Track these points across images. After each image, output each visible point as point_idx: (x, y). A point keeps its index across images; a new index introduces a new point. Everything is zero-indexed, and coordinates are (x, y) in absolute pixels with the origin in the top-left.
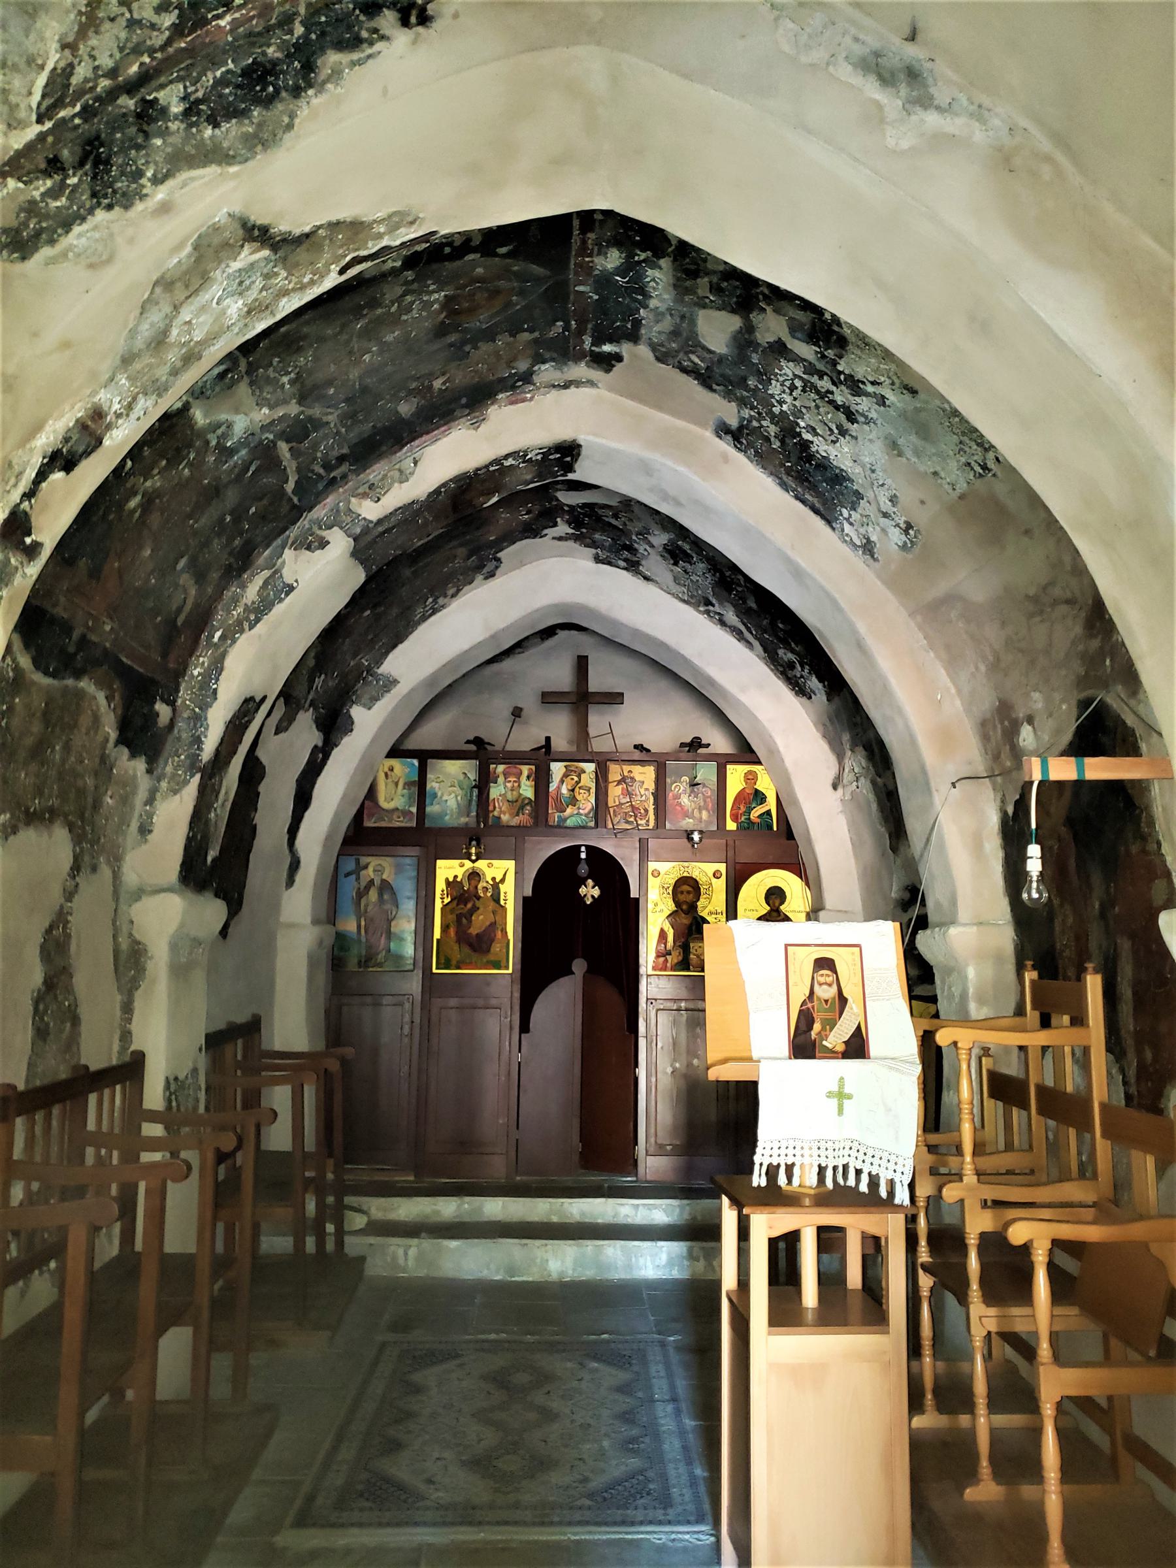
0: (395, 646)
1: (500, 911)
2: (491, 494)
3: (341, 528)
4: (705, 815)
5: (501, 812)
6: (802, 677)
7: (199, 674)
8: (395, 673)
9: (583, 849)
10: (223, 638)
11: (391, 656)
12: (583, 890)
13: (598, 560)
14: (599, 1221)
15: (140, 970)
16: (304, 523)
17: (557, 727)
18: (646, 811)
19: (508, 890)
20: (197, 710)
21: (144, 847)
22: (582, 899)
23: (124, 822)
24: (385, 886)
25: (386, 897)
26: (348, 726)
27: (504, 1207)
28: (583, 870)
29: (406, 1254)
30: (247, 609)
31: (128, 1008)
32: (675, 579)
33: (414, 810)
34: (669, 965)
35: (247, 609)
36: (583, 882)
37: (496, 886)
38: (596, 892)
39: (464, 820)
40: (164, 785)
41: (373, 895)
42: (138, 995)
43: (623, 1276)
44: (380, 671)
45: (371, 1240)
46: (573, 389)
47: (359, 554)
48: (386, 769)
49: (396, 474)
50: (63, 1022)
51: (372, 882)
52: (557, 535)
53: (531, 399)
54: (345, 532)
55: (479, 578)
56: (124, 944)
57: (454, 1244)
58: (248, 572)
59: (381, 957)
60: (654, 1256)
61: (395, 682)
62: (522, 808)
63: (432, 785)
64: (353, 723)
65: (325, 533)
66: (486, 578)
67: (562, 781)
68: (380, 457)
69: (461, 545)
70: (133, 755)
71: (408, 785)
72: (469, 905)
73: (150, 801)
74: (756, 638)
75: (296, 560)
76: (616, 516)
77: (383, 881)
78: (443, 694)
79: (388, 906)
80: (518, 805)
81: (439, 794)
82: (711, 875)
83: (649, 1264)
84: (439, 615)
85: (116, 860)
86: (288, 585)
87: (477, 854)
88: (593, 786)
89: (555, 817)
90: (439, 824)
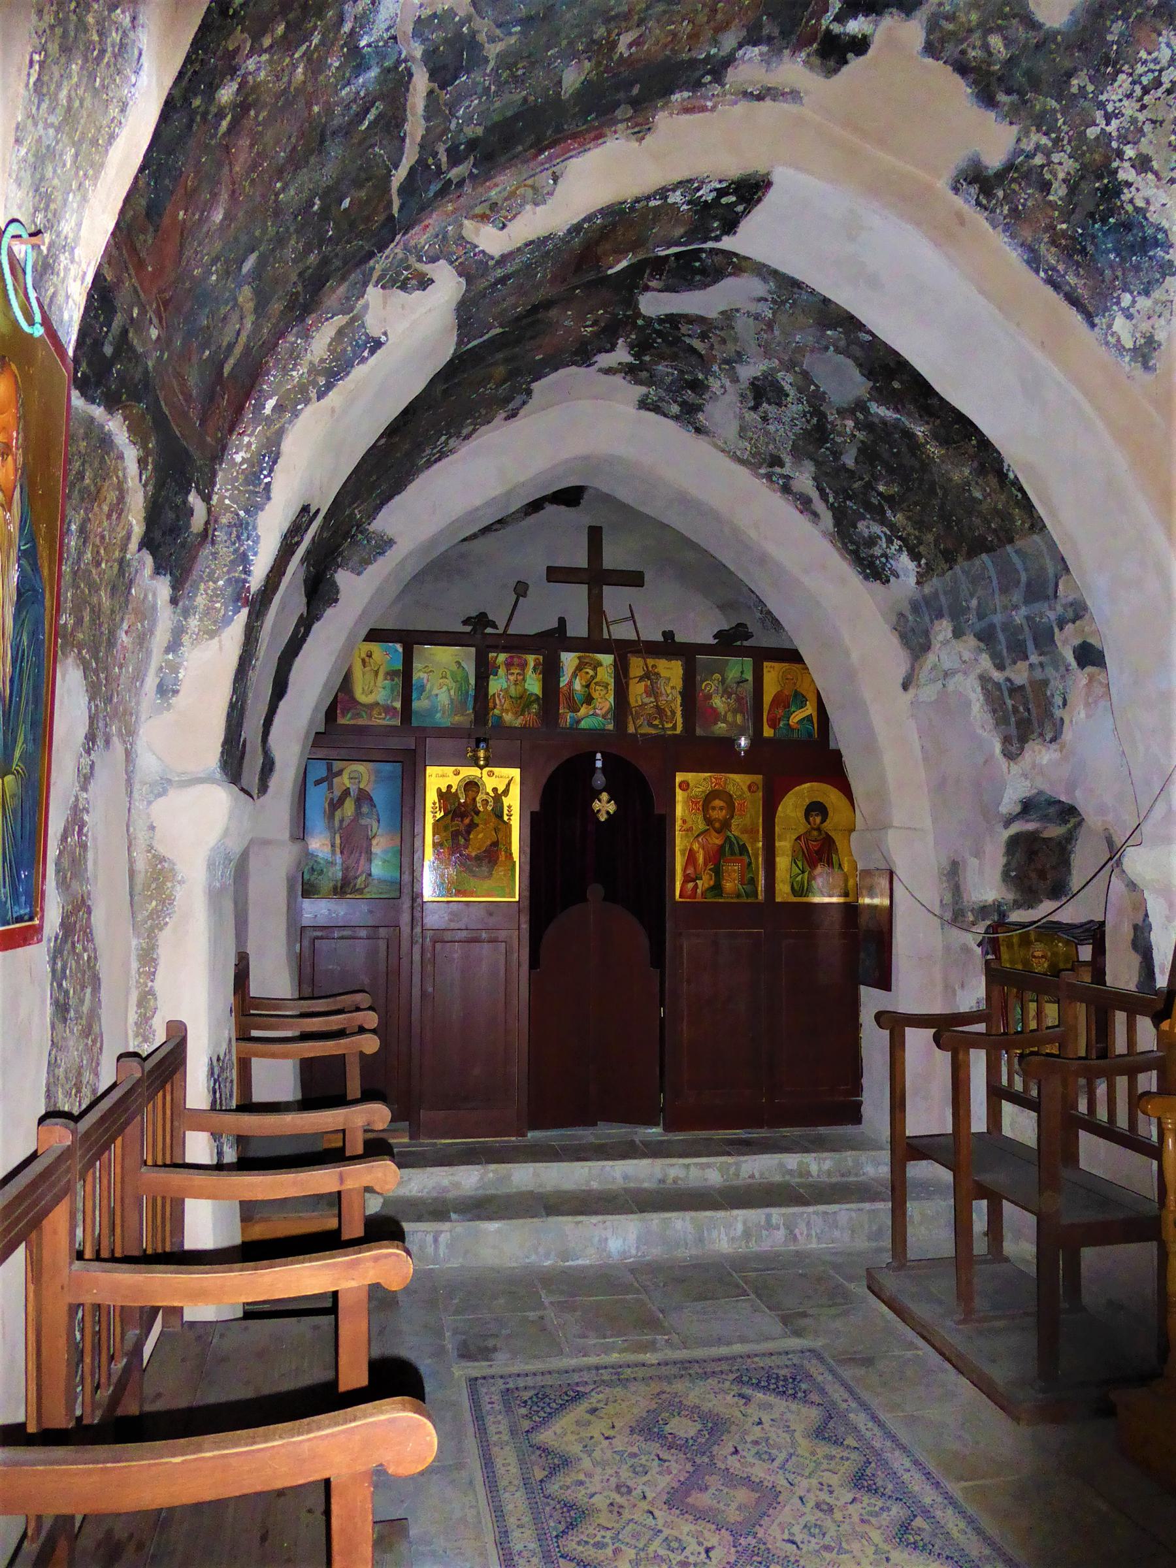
0: (390, 498)
2: (620, 253)
3: (451, 263)
4: (739, 718)
5: (502, 710)
6: (885, 555)
7: (244, 460)
8: (390, 532)
9: (599, 756)
10: (279, 408)
11: (384, 510)
13: (644, 404)
15: (166, 901)
16: (395, 250)
17: (570, 606)
18: (673, 713)
19: (513, 801)
20: (242, 513)
21: (167, 716)
22: (595, 814)
23: (139, 676)
25: (365, 809)
26: (332, 597)
27: (536, 1174)
28: (599, 780)
29: (436, 1240)
30: (313, 370)
31: (148, 958)
32: (743, 429)
33: (398, 705)
34: (699, 891)
36: (596, 795)
37: (498, 797)
38: (612, 807)
39: (457, 718)
40: (193, 623)
41: (349, 807)
42: (165, 938)
46: (768, 103)
47: (466, 314)
48: (363, 655)
49: (530, 192)
50: (83, 988)
51: (346, 792)
53: (714, 108)
54: (456, 268)
56: (141, 865)
57: (493, 1226)
58: (314, 315)
59: (360, 881)
60: (729, 1226)
61: (390, 542)
62: (528, 706)
63: (418, 675)
64: (338, 592)
66: (507, 418)
67: (574, 675)
68: (512, 161)
69: (506, 361)
70: (158, 570)
71: (391, 674)
72: (467, 821)
73: (174, 646)
74: (831, 507)
75: (385, 303)
76: (704, 336)
77: (360, 790)
78: (444, 565)
80: (523, 702)
81: (428, 687)
82: (745, 789)
83: (723, 1236)
84: (445, 461)
85: (130, 733)
87: (486, 759)
89: (567, 718)
90: (427, 723)
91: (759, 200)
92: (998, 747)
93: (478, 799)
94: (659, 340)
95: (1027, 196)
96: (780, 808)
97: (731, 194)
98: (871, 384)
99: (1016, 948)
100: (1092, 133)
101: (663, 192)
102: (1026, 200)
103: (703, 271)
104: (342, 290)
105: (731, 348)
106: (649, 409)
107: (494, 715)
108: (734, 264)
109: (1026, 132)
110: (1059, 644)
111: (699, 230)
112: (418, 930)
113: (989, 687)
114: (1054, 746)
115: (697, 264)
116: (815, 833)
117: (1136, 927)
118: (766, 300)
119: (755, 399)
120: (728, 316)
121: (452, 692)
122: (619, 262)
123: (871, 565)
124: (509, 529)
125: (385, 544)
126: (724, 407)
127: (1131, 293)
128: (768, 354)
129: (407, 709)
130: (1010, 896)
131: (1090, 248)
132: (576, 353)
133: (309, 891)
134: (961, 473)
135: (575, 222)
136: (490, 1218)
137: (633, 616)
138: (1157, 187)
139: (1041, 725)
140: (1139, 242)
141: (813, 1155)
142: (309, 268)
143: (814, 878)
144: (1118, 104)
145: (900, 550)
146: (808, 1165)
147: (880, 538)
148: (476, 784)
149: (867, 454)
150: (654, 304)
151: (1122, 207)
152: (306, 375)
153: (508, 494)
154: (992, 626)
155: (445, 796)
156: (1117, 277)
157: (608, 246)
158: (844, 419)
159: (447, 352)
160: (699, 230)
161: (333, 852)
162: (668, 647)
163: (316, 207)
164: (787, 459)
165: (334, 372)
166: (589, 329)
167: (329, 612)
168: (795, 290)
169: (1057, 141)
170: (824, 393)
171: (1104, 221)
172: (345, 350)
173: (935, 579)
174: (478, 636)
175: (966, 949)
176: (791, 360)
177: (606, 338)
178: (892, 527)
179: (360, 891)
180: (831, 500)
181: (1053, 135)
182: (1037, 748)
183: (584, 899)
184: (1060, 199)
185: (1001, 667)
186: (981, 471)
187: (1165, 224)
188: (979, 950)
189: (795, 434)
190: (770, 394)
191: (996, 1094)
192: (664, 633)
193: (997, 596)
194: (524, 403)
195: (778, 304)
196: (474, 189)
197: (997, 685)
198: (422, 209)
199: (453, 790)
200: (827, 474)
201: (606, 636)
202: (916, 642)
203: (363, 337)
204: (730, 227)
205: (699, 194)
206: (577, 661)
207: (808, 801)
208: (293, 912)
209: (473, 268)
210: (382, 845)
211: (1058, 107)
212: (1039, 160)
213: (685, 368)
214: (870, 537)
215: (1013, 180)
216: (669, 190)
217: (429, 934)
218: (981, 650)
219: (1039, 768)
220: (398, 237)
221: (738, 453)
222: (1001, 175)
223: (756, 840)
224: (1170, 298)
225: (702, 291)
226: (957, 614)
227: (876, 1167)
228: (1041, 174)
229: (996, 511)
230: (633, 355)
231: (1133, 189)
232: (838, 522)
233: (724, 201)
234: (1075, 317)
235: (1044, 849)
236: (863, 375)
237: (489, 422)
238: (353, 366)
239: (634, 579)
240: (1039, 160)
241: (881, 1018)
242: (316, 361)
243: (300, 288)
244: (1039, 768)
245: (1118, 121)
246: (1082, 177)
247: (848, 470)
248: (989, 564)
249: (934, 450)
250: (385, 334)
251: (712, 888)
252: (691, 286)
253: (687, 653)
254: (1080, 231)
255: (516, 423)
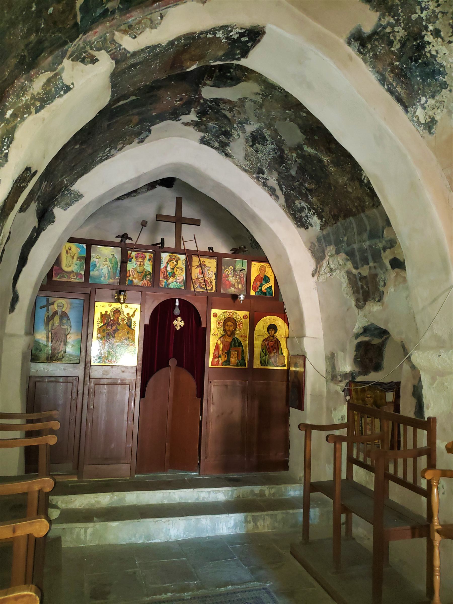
0: (82, 175)
1: (131, 331)
2: (193, 60)
3: (108, 52)
4: (240, 286)
6: (307, 216)
8: (81, 191)
9: (177, 300)
10: (14, 115)
11: (79, 181)
12: (175, 322)
13: (203, 141)
14: (190, 501)
16: (79, 42)
18: (211, 282)
19: (136, 320)
22: (174, 327)
24: (64, 315)
25: (64, 321)
27: (137, 497)
28: (177, 311)
29: (85, 532)
30: (33, 97)
32: (246, 155)
33: (83, 273)
34: (220, 362)
35: (33, 97)
36: (175, 318)
37: (129, 318)
39: (112, 280)
41: (57, 320)
43: (211, 535)
44: (72, 189)
45: (65, 526)
47: (115, 77)
48: (67, 249)
49: (149, 22)
51: (56, 313)
52: (185, 121)
54: (111, 55)
55: (136, 141)
57: (115, 524)
58: (35, 70)
61: (81, 196)
62: (145, 276)
64: (54, 217)
65: (96, 53)
66: (139, 142)
67: (168, 264)
69: (138, 114)
71: (80, 258)
72: (114, 328)
74: (284, 194)
76: (231, 110)
77: (63, 312)
79: (65, 327)
80: (143, 274)
81: (98, 265)
82: (242, 317)
84: (109, 160)
86: (66, 86)
88: (184, 267)
89: (163, 283)
90: (97, 281)
91: (259, 41)
92: (353, 303)
93: (119, 318)
94: (210, 111)
95: (381, 48)
96: (257, 327)
97: (246, 36)
98: (305, 137)
99: (359, 393)
100: (414, 17)
101: (214, 31)
102: (381, 50)
103: (231, 78)
104: (50, 59)
105: (243, 116)
106: (205, 144)
107: (129, 279)
108: (247, 74)
109: (383, 15)
110: (383, 258)
111: (230, 55)
112: (87, 379)
113: (351, 277)
114: (379, 303)
115: (229, 74)
116: (272, 338)
117: (414, 386)
118: (260, 94)
119: (252, 141)
120: (242, 100)
121: (109, 268)
122: (192, 65)
123: (301, 221)
124: (140, 196)
125: (78, 197)
126: (239, 146)
127: (426, 97)
128: (259, 120)
129: (87, 276)
130: (357, 370)
131: (409, 75)
132: (172, 114)
133: (34, 358)
134: (343, 180)
135: (171, 39)
136: (113, 520)
137: (195, 239)
138: (442, 45)
139: (374, 294)
140: (431, 72)
141: (267, 486)
142: (31, 43)
143: (271, 358)
144: (427, 4)
145: (314, 214)
146: (264, 491)
147: (305, 208)
148: (119, 311)
149: (302, 170)
150: (209, 92)
151: (425, 54)
152: (29, 100)
153: (139, 177)
154: (353, 249)
155: (104, 316)
156: (420, 89)
157: (187, 56)
158: (292, 153)
159: (105, 99)
160: (230, 55)
161: (48, 341)
162: (210, 253)
163: (33, 9)
164: (266, 171)
165: (45, 100)
166: (178, 102)
167: (50, 227)
168: (273, 90)
169: (397, 21)
170: (284, 140)
171: (416, 61)
172: (51, 90)
173: (328, 228)
174: (123, 243)
175: (337, 392)
176: (269, 123)
177: (186, 108)
178: (310, 203)
179: (60, 360)
180: (284, 190)
181: (396, 18)
182: (371, 304)
183: (167, 365)
184: (397, 50)
185: (356, 268)
186: (352, 179)
187: (445, 64)
188: (343, 394)
189: (270, 159)
190: (260, 140)
191: (351, 461)
192: (209, 248)
193: (356, 236)
194: (147, 136)
195: (265, 96)
196: (120, 16)
197: (355, 276)
198: (93, 23)
199: (108, 314)
200: (283, 178)
201: (182, 248)
202: (319, 257)
203: (61, 84)
204: (245, 54)
205: (231, 34)
206: (169, 257)
207: (269, 324)
208: (25, 369)
209: (119, 57)
210: (72, 339)
211: (399, 3)
212: (388, 30)
213: (222, 125)
214: (300, 208)
215: (376, 40)
216: (217, 30)
217: (92, 381)
218: (347, 260)
219: (374, 312)
220: (81, 36)
221: (244, 167)
222: (370, 37)
223: (246, 341)
224: (443, 100)
225: (230, 88)
226: (338, 243)
227: (295, 491)
228: (389, 37)
229: (358, 198)
230: (198, 117)
231: (431, 46)
232: (287, 200)
233: (243, 39)
234: (399, 108)
235: (372, 348)
236: (302, 133)
237: (130, 144)
238: (55, 98)
239: (196, 222)
240: (388, 30)
241: (300, 426)
242: (35, 94)
243: (26, 53)
244: (374, 312)
245: (426, 12)
246: (408, 39)
247: (293, 177)
248: (353, 221)
249: (331, 169)
250: (73, 84)
251: (225, 362)
252: (225, 85)
253: (219, 257)
254: (405, 66)
255: (143, 146)
